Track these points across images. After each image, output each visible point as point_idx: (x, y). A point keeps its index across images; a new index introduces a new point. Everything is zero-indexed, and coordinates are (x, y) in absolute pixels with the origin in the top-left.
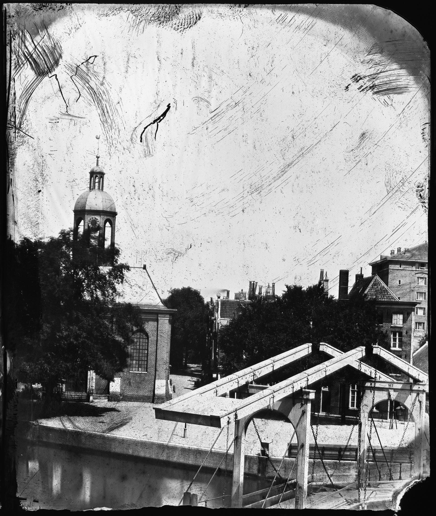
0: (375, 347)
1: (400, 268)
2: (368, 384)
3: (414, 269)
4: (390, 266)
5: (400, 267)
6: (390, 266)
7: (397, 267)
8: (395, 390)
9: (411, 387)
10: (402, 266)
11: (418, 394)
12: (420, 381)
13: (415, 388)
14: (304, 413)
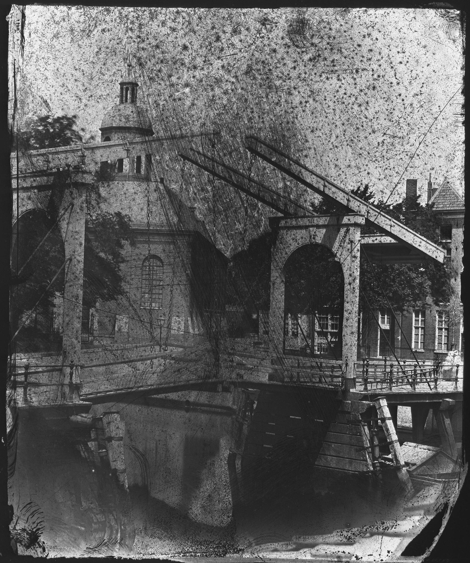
9: (338, 220)
11: (348, 231)
12: (353, 211)
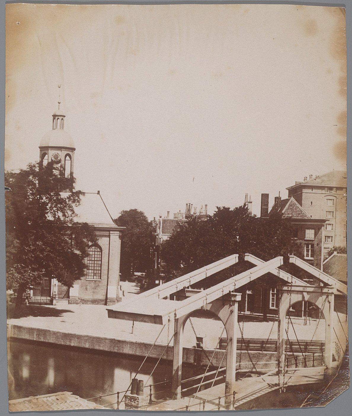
0: (291, 257)
1: (312, 192)
2: (285, 288)
3: (324, 193)
4: (303, 190)
5: (312, 191)
6: (303, 190)
7: (310, 191)
8: (308, 292)
9: (322, 290)
10: (313, 190)
11: (327, 297)
13: (325, 290)
14: (232, 312)
